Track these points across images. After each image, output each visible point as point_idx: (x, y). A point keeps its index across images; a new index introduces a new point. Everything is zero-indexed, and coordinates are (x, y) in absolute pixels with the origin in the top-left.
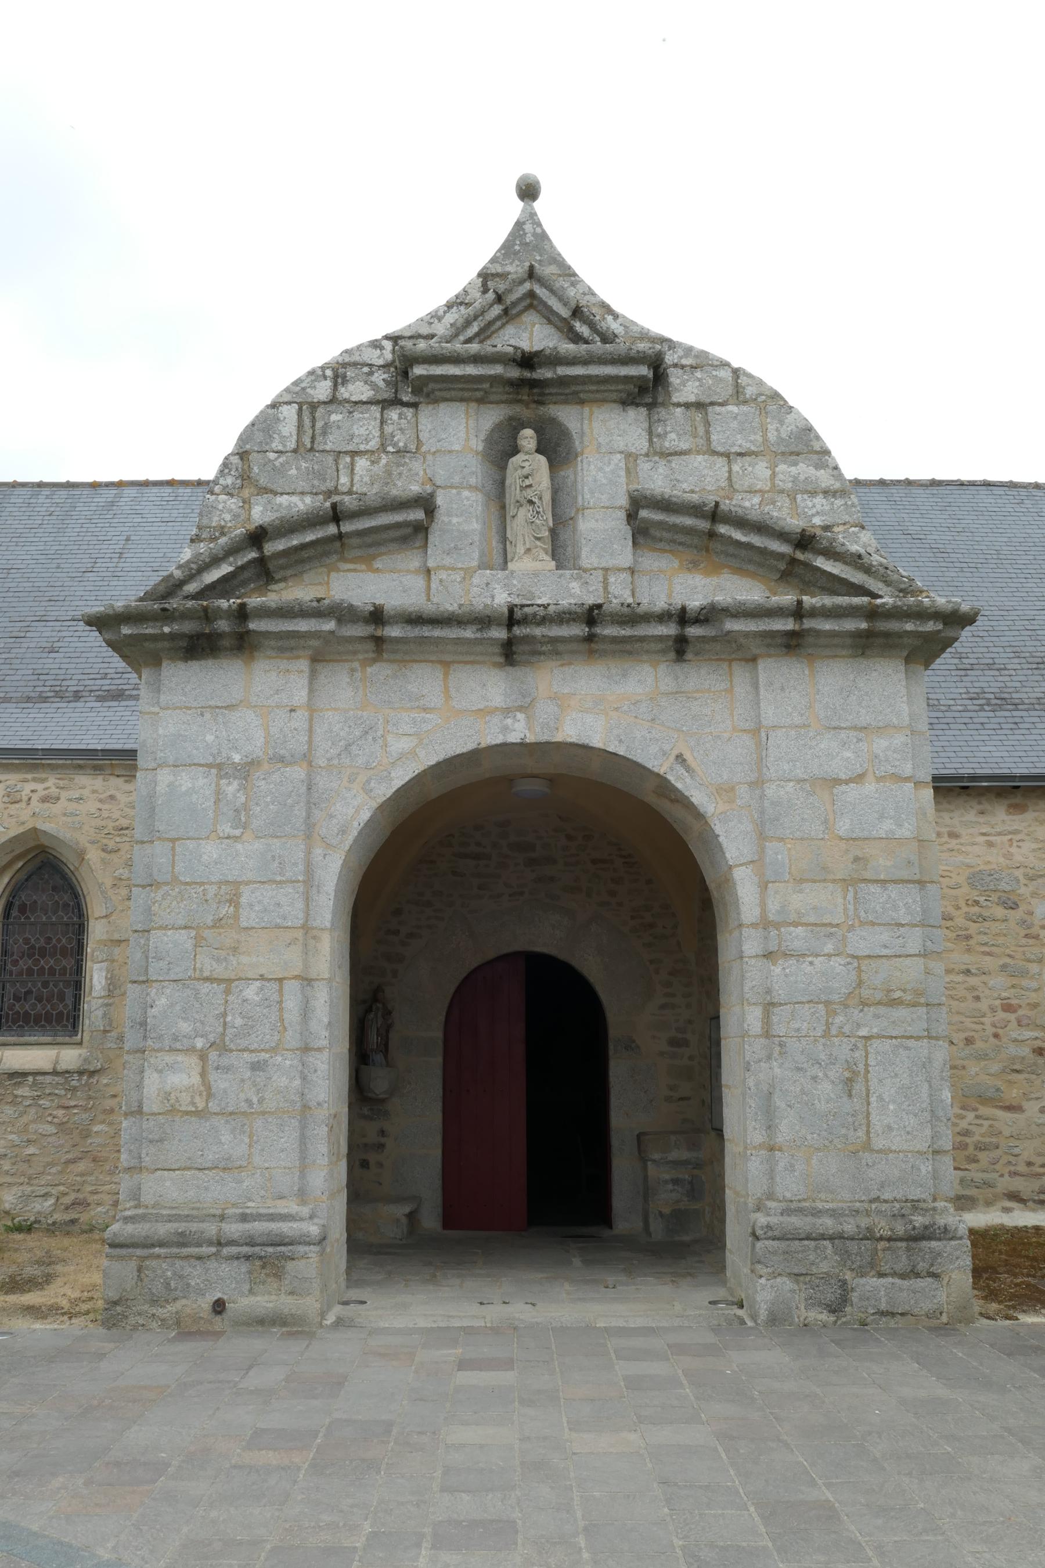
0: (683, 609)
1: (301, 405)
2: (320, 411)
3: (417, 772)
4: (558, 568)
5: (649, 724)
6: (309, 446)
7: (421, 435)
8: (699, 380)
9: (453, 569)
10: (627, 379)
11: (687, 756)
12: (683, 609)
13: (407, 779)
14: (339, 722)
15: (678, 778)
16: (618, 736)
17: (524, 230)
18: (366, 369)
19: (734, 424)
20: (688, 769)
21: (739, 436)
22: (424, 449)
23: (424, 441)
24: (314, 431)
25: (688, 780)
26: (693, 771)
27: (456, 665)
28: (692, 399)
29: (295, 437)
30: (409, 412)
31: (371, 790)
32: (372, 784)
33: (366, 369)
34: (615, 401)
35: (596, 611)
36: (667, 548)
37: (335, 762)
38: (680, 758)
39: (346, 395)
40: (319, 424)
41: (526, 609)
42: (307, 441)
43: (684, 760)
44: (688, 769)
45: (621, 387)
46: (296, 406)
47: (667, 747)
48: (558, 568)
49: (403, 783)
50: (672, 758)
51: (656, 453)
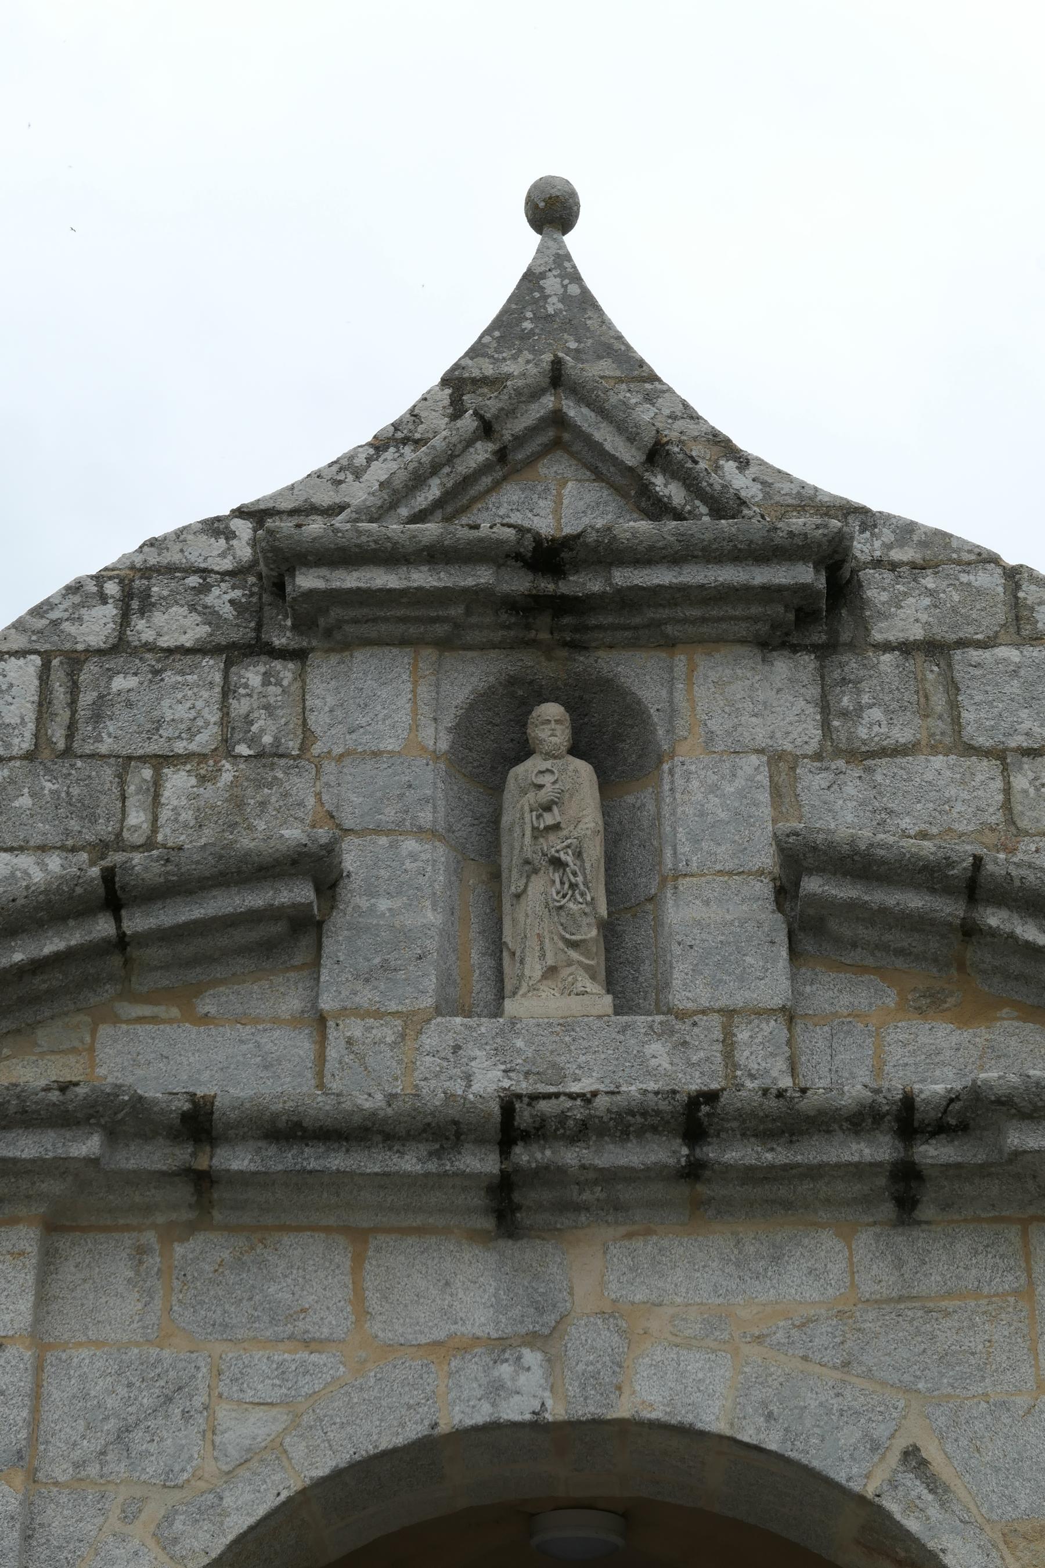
0: (908, 1102)
1: (47, 658)
2: (90, 671)
3: (283, 1497)
4: (618, 1011)
5: (837, 1375)
6: (61, 745)
7: (312, 719)
8: (931, 593)
9: (378, 1015)
10: (769, 593)
11: (931, 1451)
12: (908, 1102)
13: (261, 1511)
14: (104, 1375)
15: (911, 1507)
16: (764, 1404)
17: (542, 289)
18: (194, 580)
19: (1014, 687)
20: (933, 1484)
21: (1024, 714)
22: (317, 749)
23: (318, 731)
24: (74, 712)
25: (934, 1512)
26: (947, 1490)
27: (381, 1237)
28: (917, 633)
29: (31, 726)
30: (286, 671)
31: (175, 1541)
32: (178, 1526)
33: (194, 580)
34: (743, 641)
35: (705, 1109)
36: (870, 961)
37: (93, 1470)
38: (913, 1459)
39: (148, 636)
40: (87, 698)
41: (543, 1105)
42: (58, 735)
43: (924, 1463)
44: (933, 1484)
45: (755, 610)
46: (37, 660)
47: (881, 1431)
48: (618, 1011)
49: (251, 1521)
50: (894, 1459)
51: (838, 753)
